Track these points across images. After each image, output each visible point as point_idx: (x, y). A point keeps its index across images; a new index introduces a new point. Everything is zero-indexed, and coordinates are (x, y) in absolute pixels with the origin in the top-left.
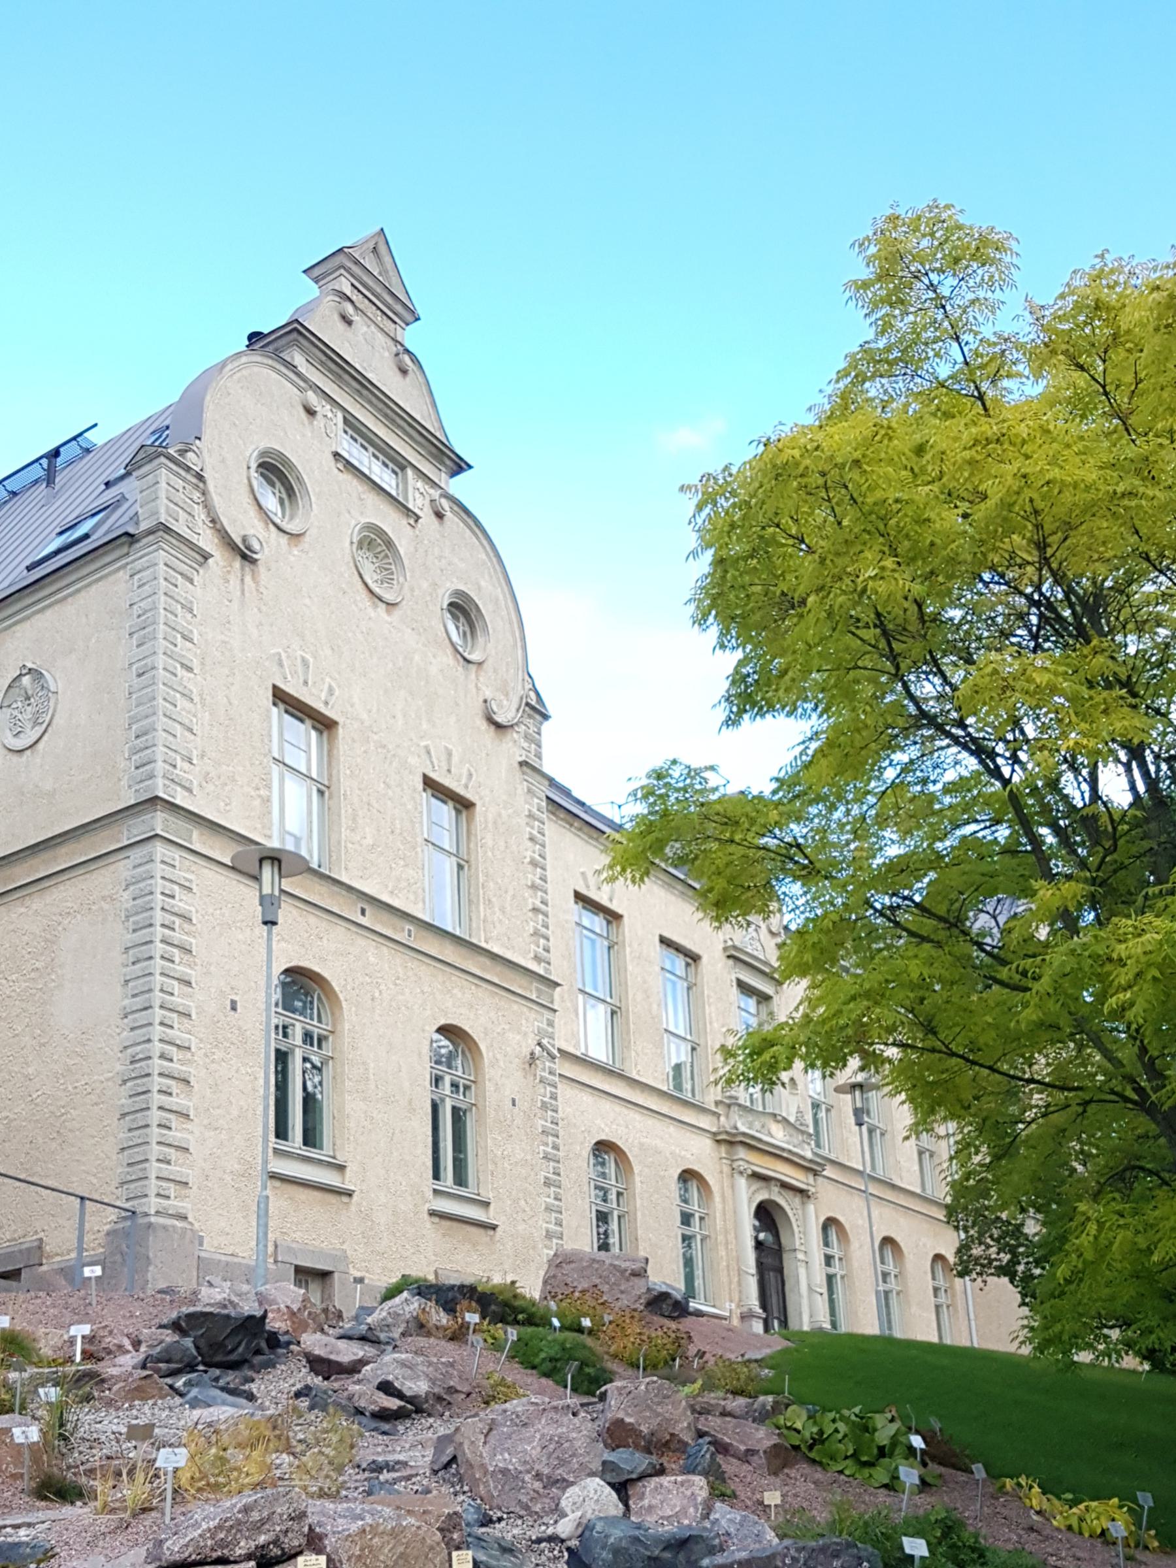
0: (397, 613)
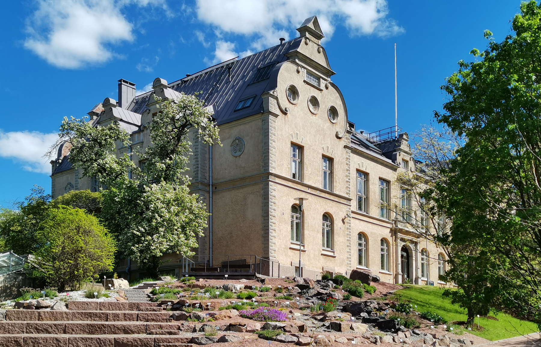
0: (317, 116)
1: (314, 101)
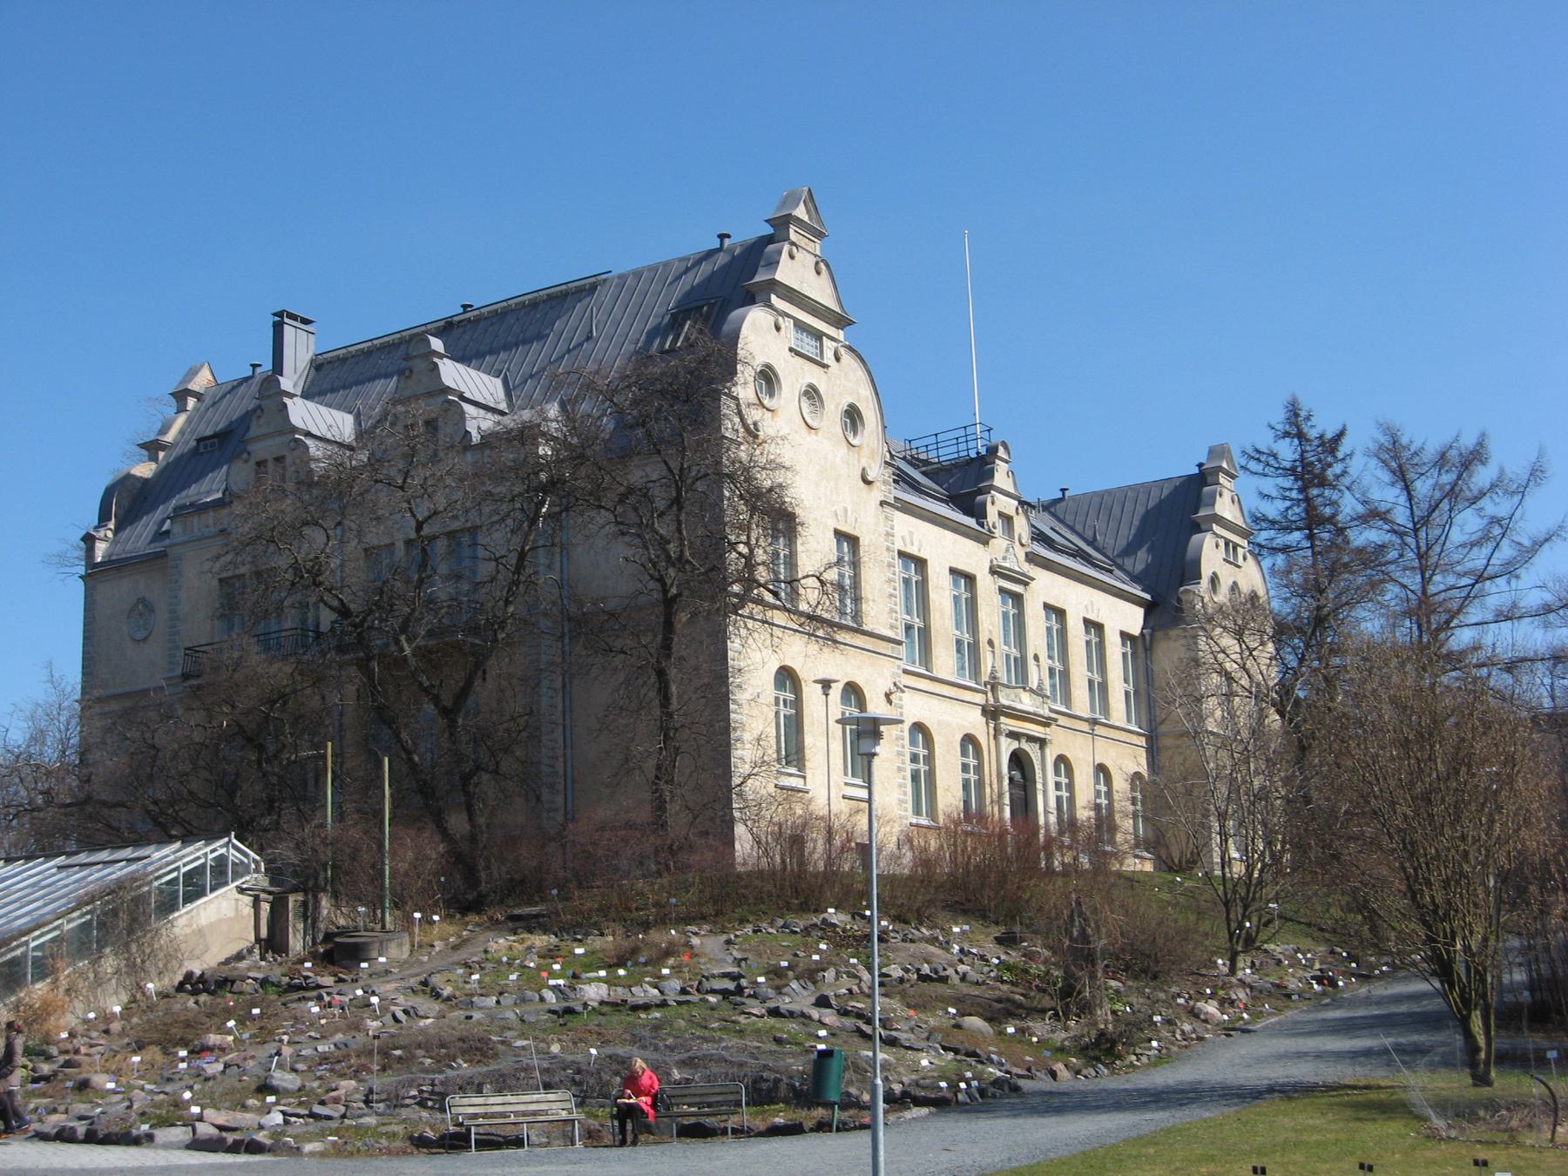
0: (820, 432)
1: (812, 393)
